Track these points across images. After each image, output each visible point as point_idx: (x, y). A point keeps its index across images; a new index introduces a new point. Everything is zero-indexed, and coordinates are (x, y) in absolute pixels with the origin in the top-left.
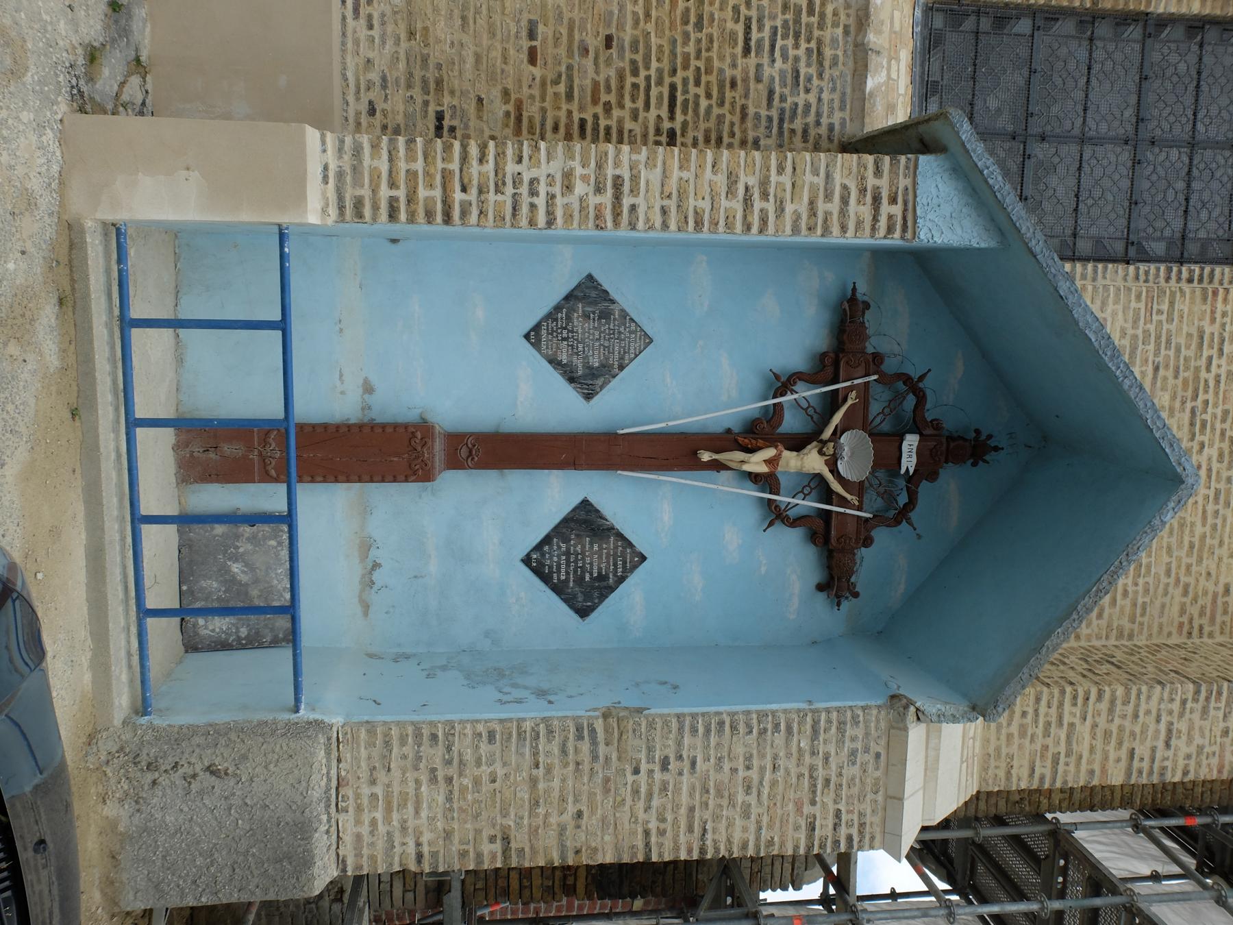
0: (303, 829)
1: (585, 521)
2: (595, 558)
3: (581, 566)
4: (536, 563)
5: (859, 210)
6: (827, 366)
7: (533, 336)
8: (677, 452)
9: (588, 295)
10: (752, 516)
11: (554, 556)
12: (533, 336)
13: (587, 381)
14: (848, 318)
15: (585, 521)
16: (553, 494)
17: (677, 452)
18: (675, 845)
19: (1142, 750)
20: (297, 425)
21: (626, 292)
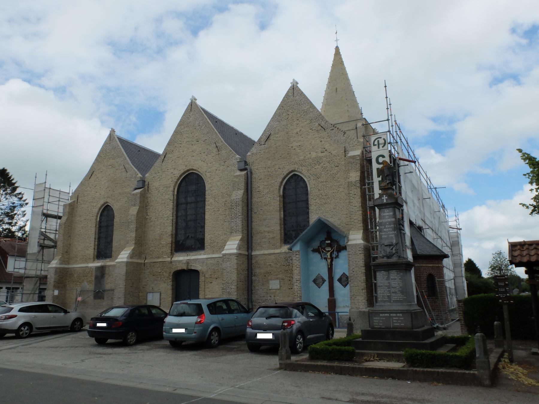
0: (360, 312)
1: (340, 280)
2: (344, 279)
3: (344, 280)
4: (345, 286)
5: (297, 256)
6: (320, 253)
7: (319, 287)
8: (330, 270)
9: (315, 281)
10: (337, 259)
11: (344, 284)
12: (319, 287)
13: (324, 281)
14: (314, 251)
15: (340, 280)
16: (337, 284)
17: (330, 270)
18: (363, 270)
19: (357, 209)
20: (61, 264)
21: (314, 277)
